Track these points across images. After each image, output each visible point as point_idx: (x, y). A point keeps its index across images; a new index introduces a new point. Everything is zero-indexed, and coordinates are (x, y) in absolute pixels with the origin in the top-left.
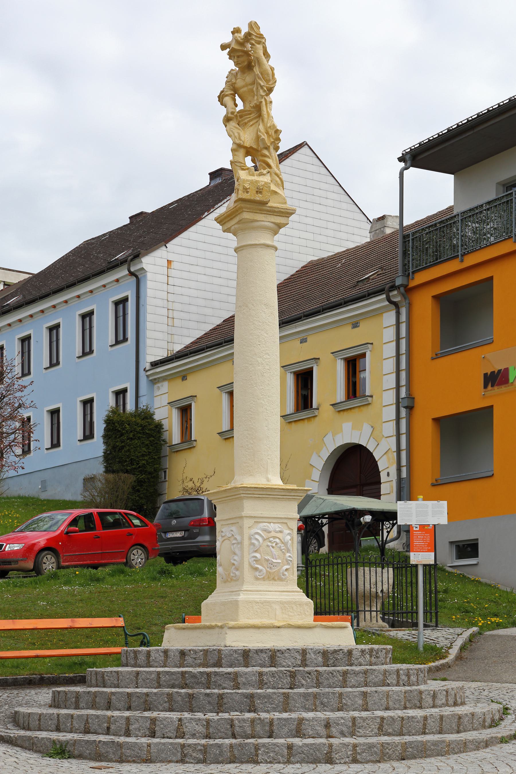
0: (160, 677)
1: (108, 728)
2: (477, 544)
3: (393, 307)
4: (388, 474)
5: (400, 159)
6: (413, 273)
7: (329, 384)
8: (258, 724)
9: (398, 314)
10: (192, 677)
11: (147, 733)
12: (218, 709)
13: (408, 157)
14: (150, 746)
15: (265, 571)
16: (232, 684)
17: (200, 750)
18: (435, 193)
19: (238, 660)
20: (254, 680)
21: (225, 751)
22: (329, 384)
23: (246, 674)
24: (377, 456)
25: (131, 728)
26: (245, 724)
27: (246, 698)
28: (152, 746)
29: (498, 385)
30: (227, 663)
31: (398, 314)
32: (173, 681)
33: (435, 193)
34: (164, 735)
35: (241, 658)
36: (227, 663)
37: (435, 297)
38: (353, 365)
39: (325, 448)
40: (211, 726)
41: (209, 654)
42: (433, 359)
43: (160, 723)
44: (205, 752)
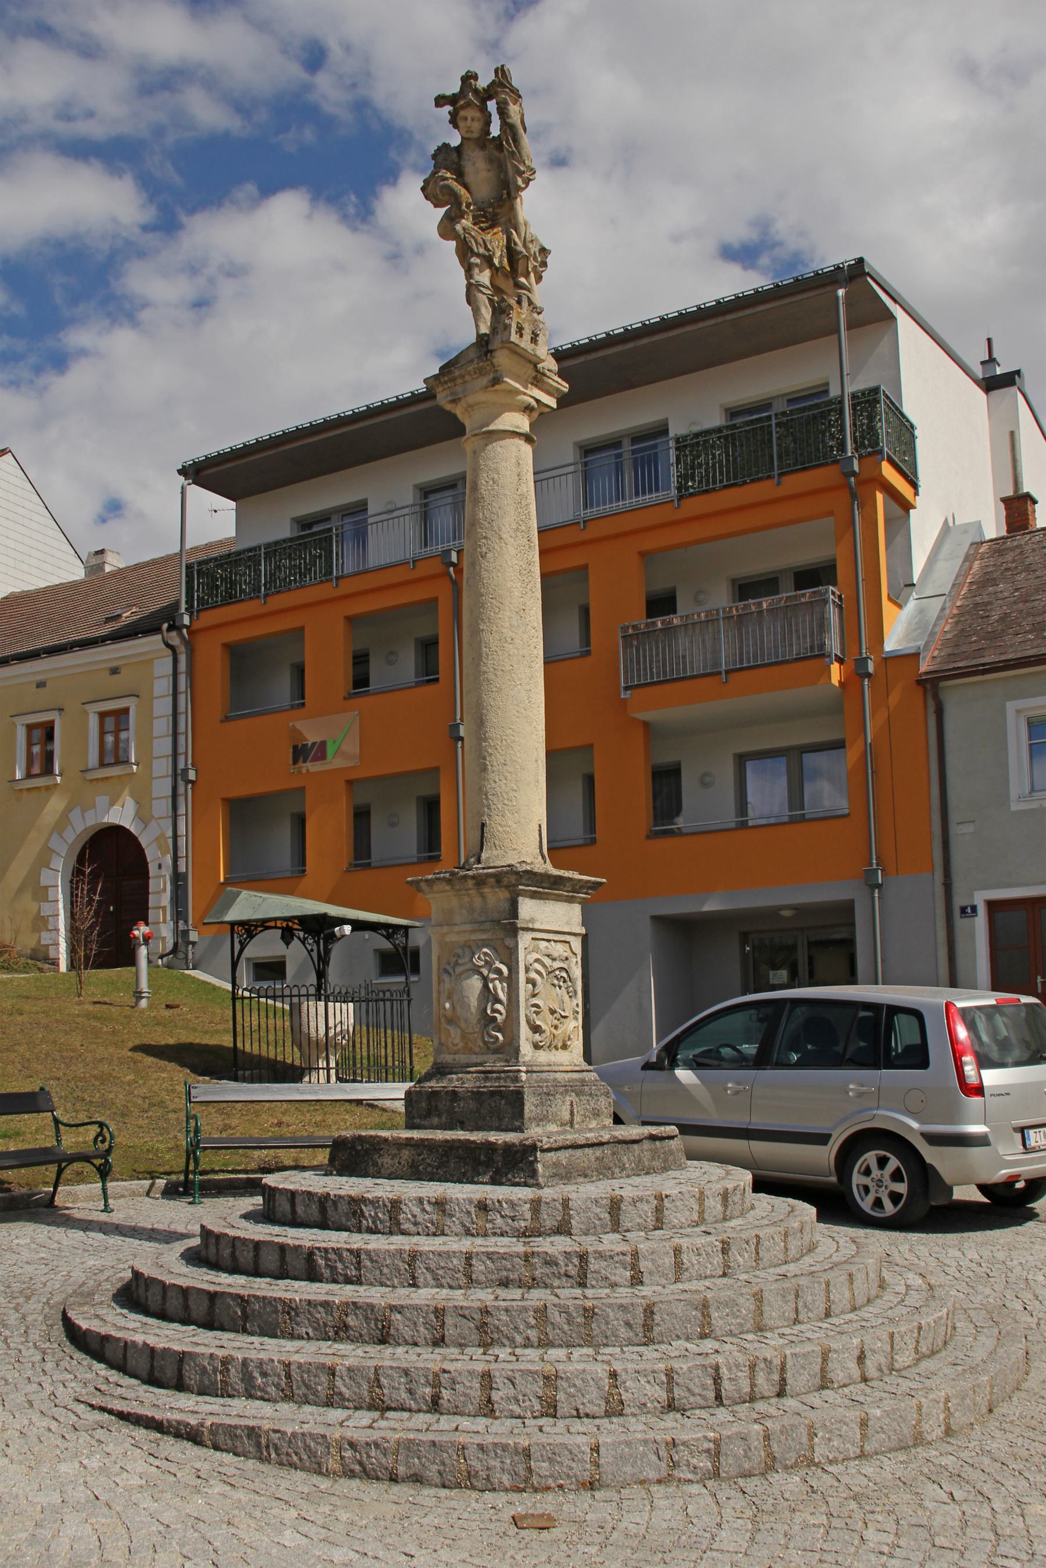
0: (471, 1265)
1: (436, 1400)
2: (284, 962)
3: (170, 652)
4: (160, 867)
5: (181, 472)
6: (198, 611)
7: (78, 743)
8: (762, 1370)
9: (175, 662)
10: (547, 1263)
11: (537, 1407)
12: (645, 1336)
13: (191, 472)
14: (598, 1452)
15: (548, 1033)
16: (628, 1273)
17: (708, 1451)
18: (215, 520)
19: (600, 1219)
20: (668, 1264)
21: (756, 1448)
22: (78, 743)
23: (653, 1253)
24: (143, 841)
25: (495, 1396)
26: (740, 1374)
27: (696, 1309)
28: (602, 1450)
29: (312, 760)
30: (580, 1226)
31: (175, 662)
32: (505, 1273)
33: (215, 520)
34: (577, 1410)
35: (607, 1215)
36: (580, 1226)
37: (226, 646)
38: (116, 720)
39: (70, 827)
40: (677, 1384)
41: (543, 1207)
42: (222, 721)
43: (565, 1384)
44: (718, 1454)
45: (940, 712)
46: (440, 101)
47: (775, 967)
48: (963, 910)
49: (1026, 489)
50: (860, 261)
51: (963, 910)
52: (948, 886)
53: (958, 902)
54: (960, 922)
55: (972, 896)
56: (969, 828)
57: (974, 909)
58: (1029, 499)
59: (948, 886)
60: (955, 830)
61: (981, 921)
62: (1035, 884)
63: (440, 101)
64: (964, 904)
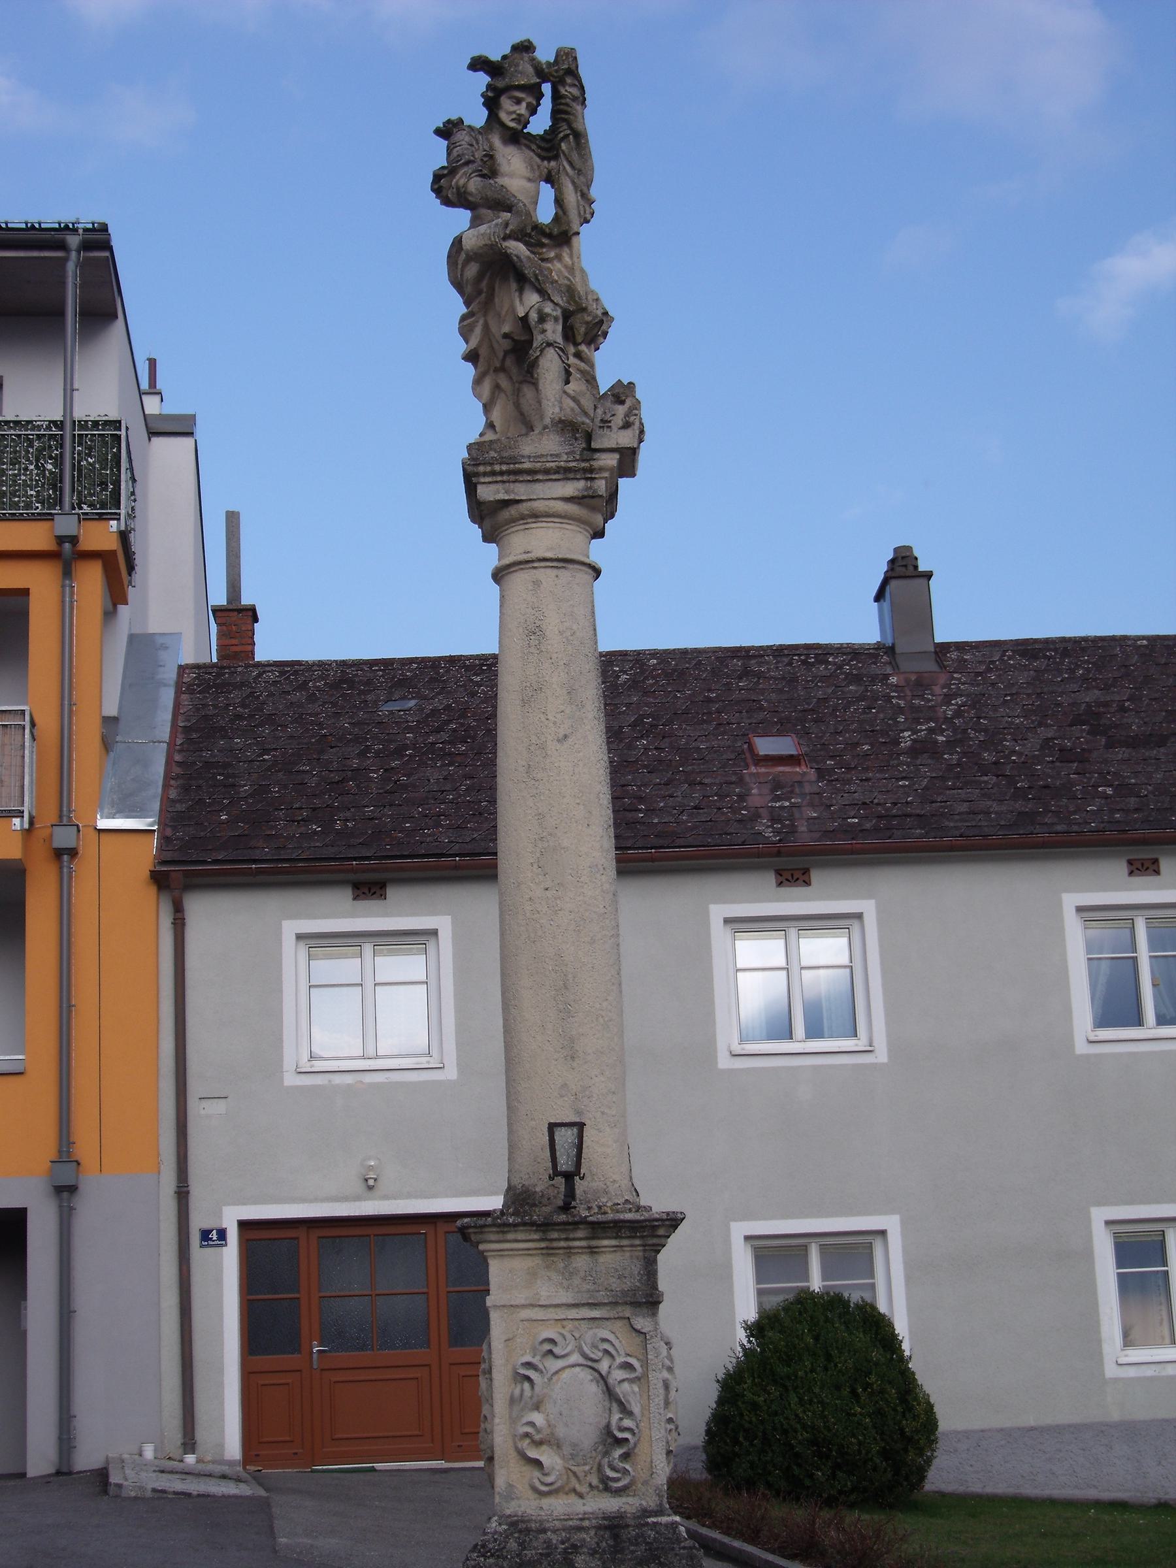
45: (179, 925)
46: (479, 64)
47: (155, 1450)
48: (205, 1235)
49: (246, 600)
50: (631, 385)
51: (205, 1235)
52: (182, 1195)
53: (198, 1222)
54: (197, 1251)
55: (220, 1216)
56: (219, 1107)
57: (222, 1234)
58: (252, 614)
59: (182, 1195)
60: (195, 1107)
61: (230, 1255)
62: (316, 1200)
63: (479, 64)
64: (206, 1226)
